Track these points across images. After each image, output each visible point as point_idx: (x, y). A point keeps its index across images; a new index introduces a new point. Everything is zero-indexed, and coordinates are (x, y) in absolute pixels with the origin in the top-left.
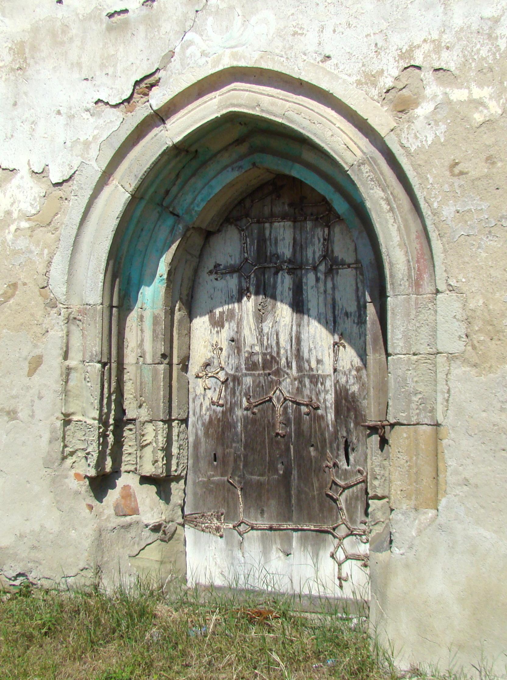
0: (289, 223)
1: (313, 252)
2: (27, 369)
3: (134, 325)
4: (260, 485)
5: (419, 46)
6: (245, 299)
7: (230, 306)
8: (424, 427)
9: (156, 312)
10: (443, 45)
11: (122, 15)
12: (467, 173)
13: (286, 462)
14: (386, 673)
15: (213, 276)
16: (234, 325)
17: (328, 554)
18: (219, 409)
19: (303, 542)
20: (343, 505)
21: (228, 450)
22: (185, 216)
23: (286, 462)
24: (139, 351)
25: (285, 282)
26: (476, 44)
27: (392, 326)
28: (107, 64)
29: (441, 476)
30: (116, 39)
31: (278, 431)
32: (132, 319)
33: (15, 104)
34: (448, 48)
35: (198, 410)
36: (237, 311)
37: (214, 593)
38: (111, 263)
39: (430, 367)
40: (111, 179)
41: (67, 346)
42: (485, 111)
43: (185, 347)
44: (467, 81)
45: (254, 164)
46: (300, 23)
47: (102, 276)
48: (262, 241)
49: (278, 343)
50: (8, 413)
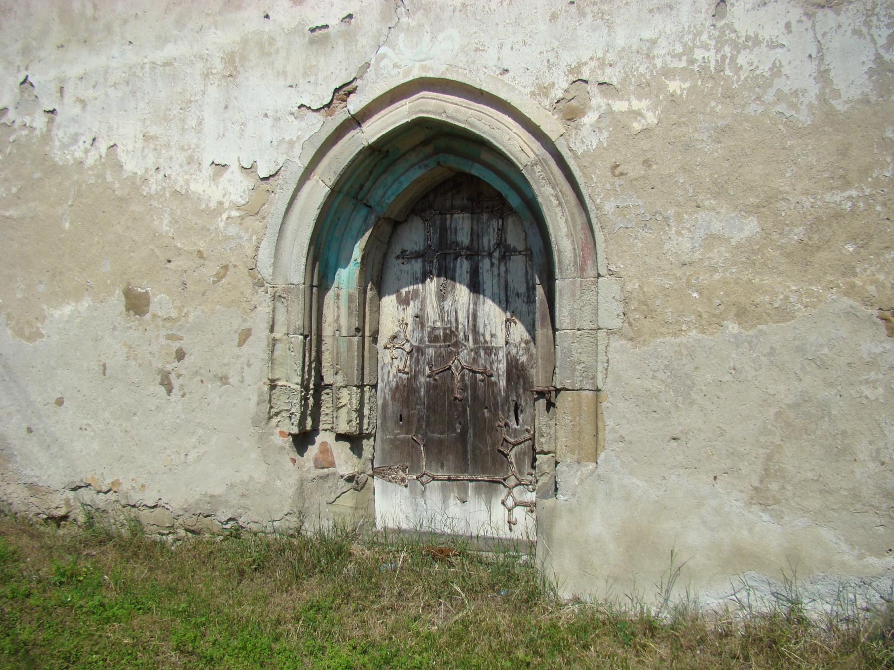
0: (467, 215)
1: (489, 240)
2: (238, 340)
3: (332, 303)
4: (440, 442)
5: (586, 63)
7: (415, 287)
9: (351, 291)
12: (626, 174)
14: (551, 601)
15: (401, 260)
16: (418, 303)
17: (500, 501)
18: (405, 376)
19: (478, 491)
20: (513, 460)
23: (463, 422)
25: (463, 266)
29: (600, 433)
32: (331, 294)
33: (227, 107)
34: (611, 65)
35: (386, 377)
37: (401, 535)
38: (312, 248)
39: (592, 340)
41: (273, 321)
42: (643, 121)
44: (628, 95)
45: (438, 163)
47: (304, 260)
48: (443, 231)
49: (457, 319)
50: (221, 379)
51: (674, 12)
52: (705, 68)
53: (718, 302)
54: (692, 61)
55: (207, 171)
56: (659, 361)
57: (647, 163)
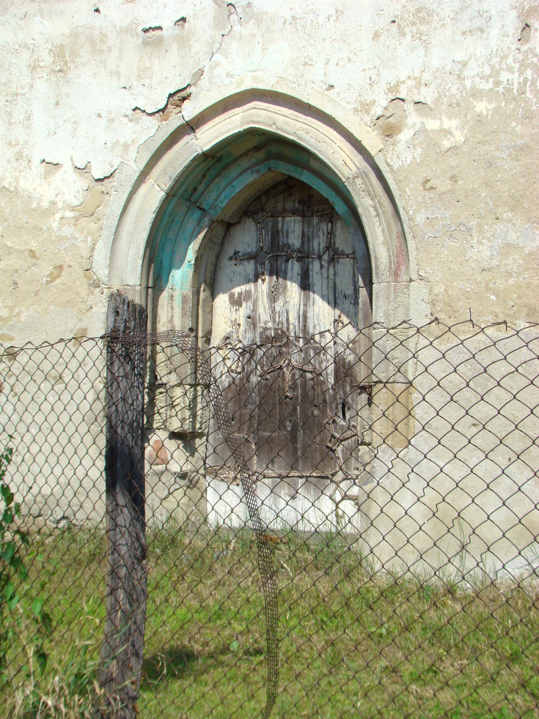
0: (298, 218)
1: (319, 243)
3: (165, 303)
5: (404, 82)
6: (260, 281)
8: (399, 385)
9: (185, 292)
10: (423, 82)
11: (156, 31)
12: (435, 188)
13: (293, 417)
15: (233, 262)
16: (250, 304)
20: (340, 455)
21: (244, 411)
22: (210, 211)
24: (170, 325)
25: (295, 267)
26: (448, 83)
27: (376, 306)
28: (143, 76)
30: (152, 54)
31: (287, 394)
32: (164, 297)
33: (57, 104)
34: (426, 85)
36: (253, 292)
38: (148, 250)
40: (148, 178)
42: (452, 139)
43: (208, 323)
45: (270, 169)
46: (310, 55)
47: (140, 262)
48: (275, 233)
49: (288, 320)
51: (484, 35)
52: (509, 90)
53: (512, 303)
54: (497, 83)
55: (38, 169)
56: (461, 356)
57: (454, 179)
